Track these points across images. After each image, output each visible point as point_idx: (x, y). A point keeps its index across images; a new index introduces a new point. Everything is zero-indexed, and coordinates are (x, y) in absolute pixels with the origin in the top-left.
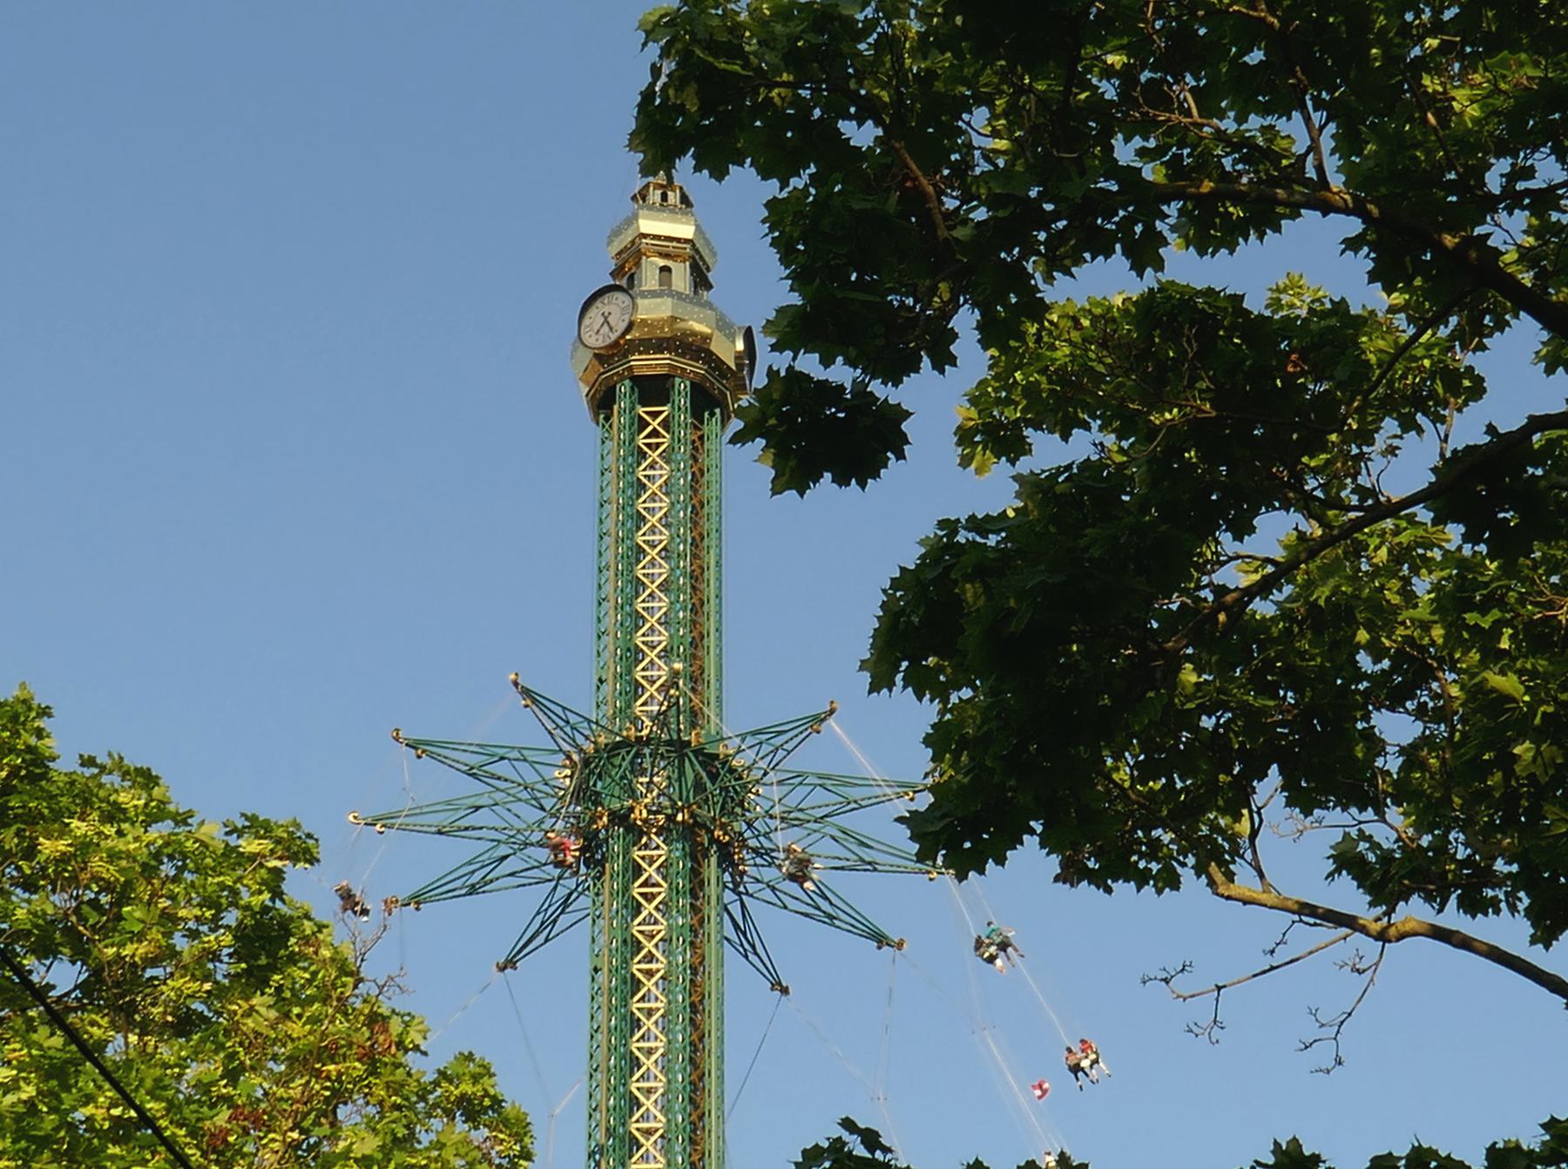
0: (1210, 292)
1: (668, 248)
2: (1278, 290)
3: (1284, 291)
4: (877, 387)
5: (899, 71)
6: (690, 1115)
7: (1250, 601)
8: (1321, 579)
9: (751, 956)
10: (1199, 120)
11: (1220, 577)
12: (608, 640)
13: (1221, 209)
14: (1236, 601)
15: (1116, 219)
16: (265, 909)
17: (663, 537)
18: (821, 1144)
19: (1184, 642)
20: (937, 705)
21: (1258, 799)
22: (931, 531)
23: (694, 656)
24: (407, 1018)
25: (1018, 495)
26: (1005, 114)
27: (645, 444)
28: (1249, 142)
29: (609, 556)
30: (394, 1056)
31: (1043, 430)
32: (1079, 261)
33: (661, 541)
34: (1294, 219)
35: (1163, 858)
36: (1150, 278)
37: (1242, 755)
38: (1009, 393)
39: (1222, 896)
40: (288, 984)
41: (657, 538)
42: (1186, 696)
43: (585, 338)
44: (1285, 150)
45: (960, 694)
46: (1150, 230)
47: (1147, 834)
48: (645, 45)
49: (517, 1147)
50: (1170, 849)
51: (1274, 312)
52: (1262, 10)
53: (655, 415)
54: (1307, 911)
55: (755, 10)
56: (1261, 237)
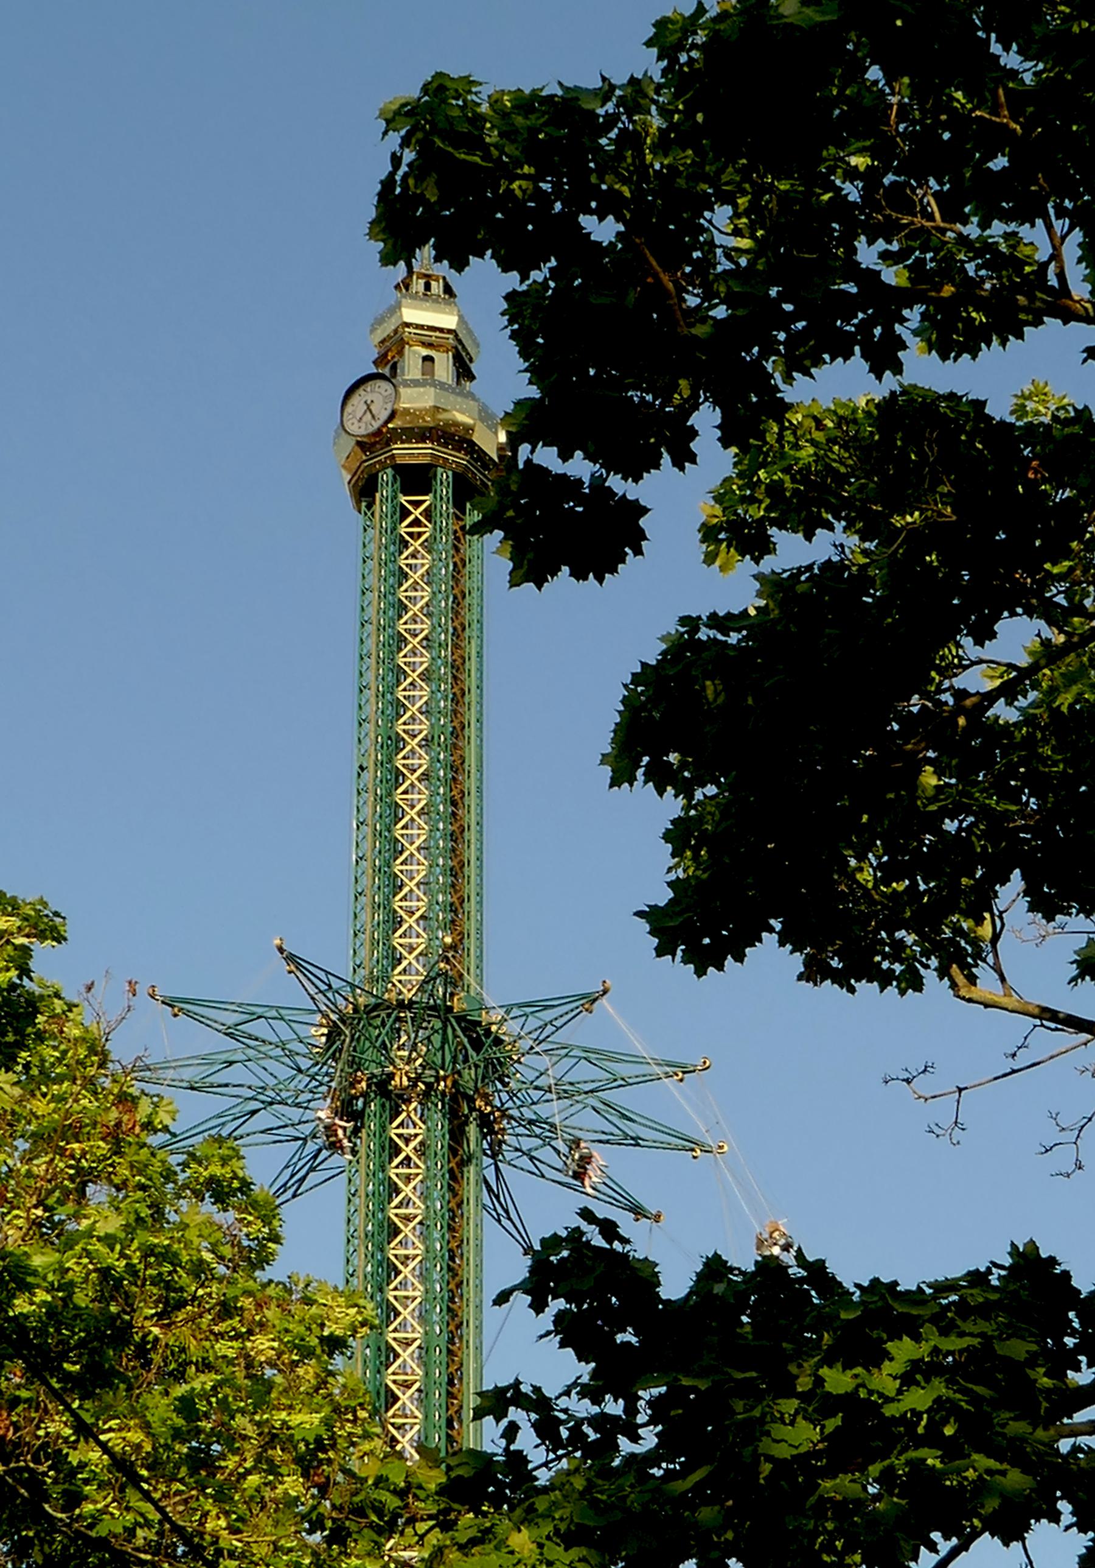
0: (952, 396)
1: (431, 337)
2: (1023, 396)
3: (1029, 398)
4: (616, 483)
5: (642, 168)
6: (449, 1202)
7: (990, 706)
8: (1065, 686)
9: (504, 1221)
10: (942, 225)
11: (959, 682)
12: (369, 727)
13: (964, 314)
14: (975, 705)
15: (855, 321)
16: (13, 987)
17: (424, 626)
18: (560, 1233)
19: (923, 745)
20: (681, 801)
21: (1000, 904)
22: (672, 627)
23: (455, 746)
24: (155, 1099)
25: (759, 595)
26: (747, 213)
27: (407, 533)
28: (992, 248)
29: (371, 644)
30: (138, 1136)
31: (787, 530)
32: (818, 362)
33: (422, 630)
34: (1036, 327)
35: (907, 959)
36: (890, 382)
37: (983, 859)
38: (752, 490)
39: (963, 998)
40: (36, 1061)
41: (418, 626)
42: (926, 798)
43: (348, 426)
44: (1028, 257)
45: (705, 790)
46: (889, 331)
47: (890, 935)
48: (385, 133)
49: (266, 1230)
50: (913, 951)
51: (1018, 419)
52: (1005, 117)
53: (417, 504)
54: (1048, 1015)
55: (496, 101)
56: (1004, 343)
